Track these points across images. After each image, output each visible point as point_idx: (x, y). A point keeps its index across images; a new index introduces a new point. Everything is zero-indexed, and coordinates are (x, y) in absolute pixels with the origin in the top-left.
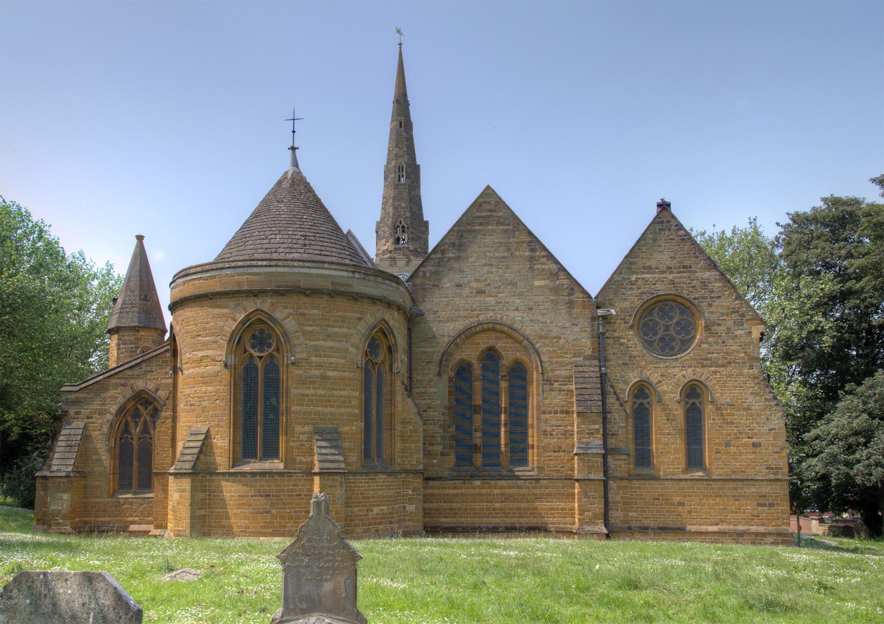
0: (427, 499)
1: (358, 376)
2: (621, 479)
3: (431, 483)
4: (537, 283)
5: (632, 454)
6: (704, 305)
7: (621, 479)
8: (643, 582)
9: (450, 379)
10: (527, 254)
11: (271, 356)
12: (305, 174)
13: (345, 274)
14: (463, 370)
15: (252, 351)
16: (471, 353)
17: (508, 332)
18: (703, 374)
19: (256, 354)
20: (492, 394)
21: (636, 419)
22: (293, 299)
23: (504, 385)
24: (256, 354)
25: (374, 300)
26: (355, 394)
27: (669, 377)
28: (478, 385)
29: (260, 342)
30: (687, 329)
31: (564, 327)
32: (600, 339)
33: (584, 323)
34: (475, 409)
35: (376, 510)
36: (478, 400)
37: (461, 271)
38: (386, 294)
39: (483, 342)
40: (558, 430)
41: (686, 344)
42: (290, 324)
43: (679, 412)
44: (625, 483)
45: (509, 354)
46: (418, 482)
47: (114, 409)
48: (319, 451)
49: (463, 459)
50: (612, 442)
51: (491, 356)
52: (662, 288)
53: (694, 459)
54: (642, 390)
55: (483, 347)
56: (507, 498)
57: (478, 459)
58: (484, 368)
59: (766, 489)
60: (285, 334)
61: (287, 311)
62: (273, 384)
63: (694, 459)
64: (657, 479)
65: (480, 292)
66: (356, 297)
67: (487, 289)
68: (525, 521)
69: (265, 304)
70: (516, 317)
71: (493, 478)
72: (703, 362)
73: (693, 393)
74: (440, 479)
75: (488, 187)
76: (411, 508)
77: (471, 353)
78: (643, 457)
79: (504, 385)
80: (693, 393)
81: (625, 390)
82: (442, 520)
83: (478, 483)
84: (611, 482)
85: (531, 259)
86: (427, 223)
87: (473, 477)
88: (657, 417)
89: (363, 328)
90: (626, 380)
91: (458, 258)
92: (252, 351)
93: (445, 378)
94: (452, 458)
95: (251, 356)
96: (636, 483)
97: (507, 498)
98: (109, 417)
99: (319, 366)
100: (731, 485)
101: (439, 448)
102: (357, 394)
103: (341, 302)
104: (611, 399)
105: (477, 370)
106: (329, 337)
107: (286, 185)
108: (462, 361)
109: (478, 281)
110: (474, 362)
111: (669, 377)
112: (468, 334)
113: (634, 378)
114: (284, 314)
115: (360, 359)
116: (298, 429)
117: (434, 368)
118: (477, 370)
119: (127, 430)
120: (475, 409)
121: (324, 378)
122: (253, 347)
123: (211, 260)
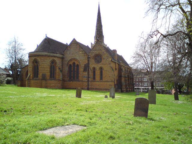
2: (91, 81)
4: (80, 53)
7: (91, 81)
12: (48, 37)
13: (47, 53)
14: (70, 65)
16: (71, 63)
17: (75, 59)
18: (102, 66)
25: (52, 56)
28: (72, 68)
30: (101, 59)
35: (52, 85)
36: (72, 70)
39: (73, 62)
40: (83, 74)
41: (101, 61)
42: (39, 60)
45: (76, 63)
51: (74, 63)
52: (97, 53)
53: (101, 78)
54: (94, 68)
56: (75, 84)
57: (72, 78)
58: (73, 65)
59: (110, 83)
63: (101, 78)
64: (96, 81)
65: (72, 54)
66: (49, 56)
70: (77, 58)
71: (74, 81)
72: (103, 64)
73: (101, 69)
75: (74, 39)
76: (59, 85)
78: (94, 78)
80: (101, 69)
86: (74, 42)
88: (96, 72)
89: (50, 60)
90: (92, 66)
93: (68, 67)
94: (69, 78)
96: (93, 82)
97: (75, 84)
99: (43, 66)
103: (46, 57)
104: (90, 70)
105: (72, 65)
111: (97, 66)
112: (71, 60)
114: (39, 59)
116: (40, 74)
117: (66, 65)
118: (72, 65)
121: (44, 67)
123: (33, 51)
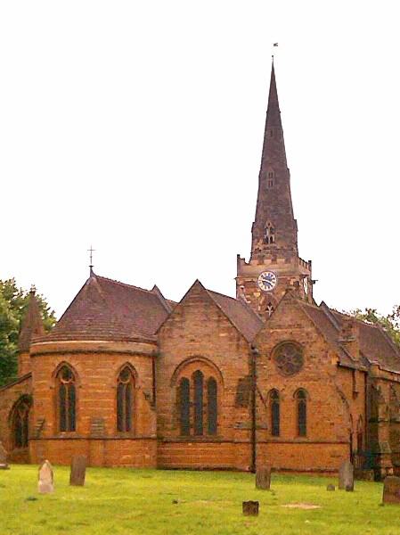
0: (160, 452)
1: (114, 392)
3: (167, 445)
4: (222, 335)
5: (269, 428)
6: (308, 347)
7: (263, 443)
8: (7, 485)
9: (178, 389)
10: (217, 318)
11: (71, 383)
13: (105, 342)
14: (185, 382)
15: (62, 380)
16: (187, 374)
18: (305, 385)
19: (64, 382)
20: (198, 396)
21: (272, 410)
22: (81, 356)
23: (205, 391)
24: (64, 382)
26: (112, 401)
27: (287, 387)
29: (66, 376)
31: (234, 360)
32: (253, 365)
33: (246, 358)
34: (191, 405)
37: (182, 328)
38: (129, 349)
39: (194, 368)
42: (78, 368)
43: (294, 405)
44: (264, 445)
45: (207, 374)
46: (154, 445)
47: (11, 405)
48: (287, 394)
49: (185, 431)
50: (258, 423)
52: (286, 337)
53: (301, 429)
55: (195, 370)
57: (192, 431)
58: (195, 382)
59: (337, 448)
60: (76, 373)
61: (77, 362)
62: (73, 399)
63: (301, 429)
66: (111, 353)
67: (196, 339)
68: (185, 464)
69: (67, 359)
72: (307, 379)
73: (301, 394)
74: (171, 442)
76: (147, 456)
77: (187, 374)
78: (275, 431)
79: (205, 391)
80: (301, 394)
81: (264, 392)
82: (173, 464)
83: (190, 444)
84: (257, 445)
85: (219, 321)
87: (188, 441)
90: (264, 388)
91: (182, 322)
92: (62, 380)
95: (62, 383)
96: (270, 445)
98: (9, 409)
99: (93, 387)
100: (318, 445)
101: (170, 426)
102: (112, 401)
104: (258, 399)
105: (191, 382)
106: (97, 373)
107: (86, 288)
108: (183, 378)
109: (191, 333)
110: (190, 379)
112: (186, 363)
113: (269, 387)
115: (116, 385)
118: (191, 382)
119: (18, 416)
120: (191, 405)
122: (63, 378)
